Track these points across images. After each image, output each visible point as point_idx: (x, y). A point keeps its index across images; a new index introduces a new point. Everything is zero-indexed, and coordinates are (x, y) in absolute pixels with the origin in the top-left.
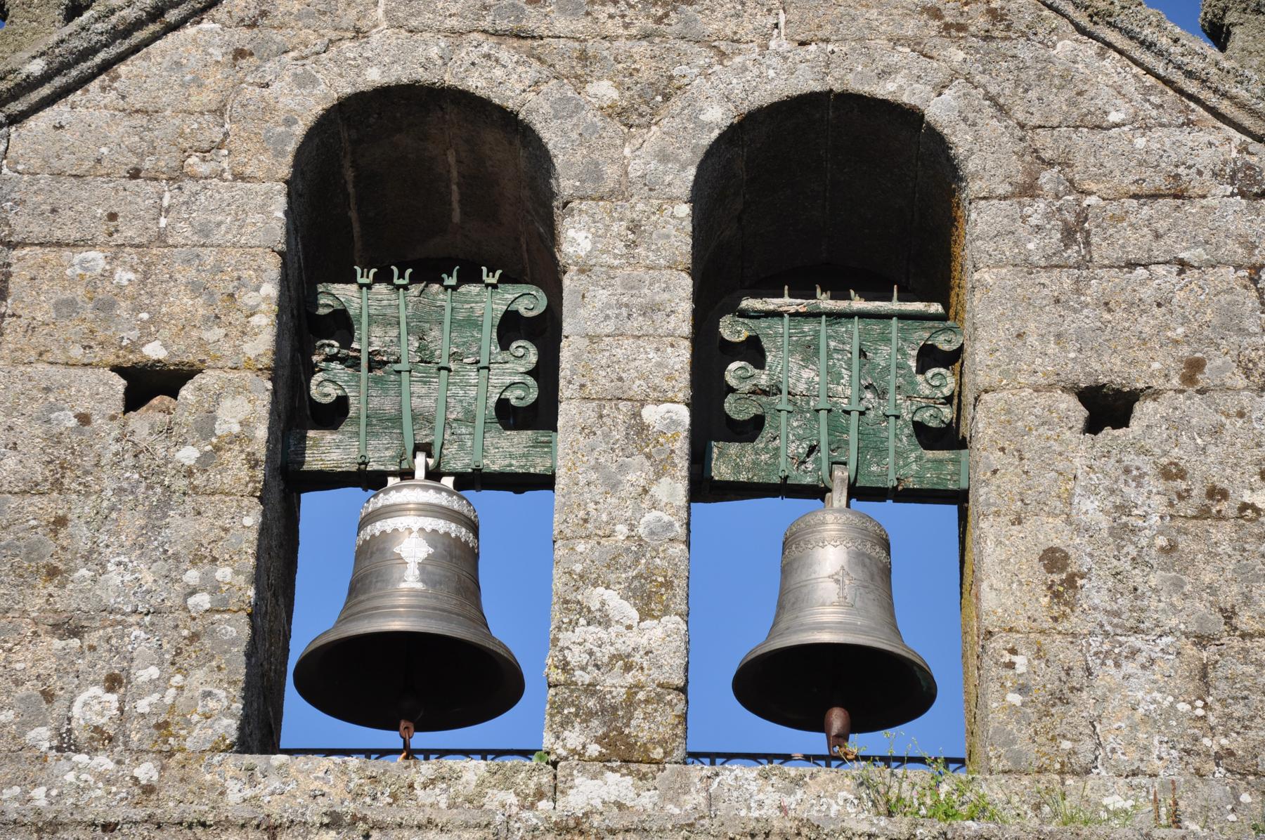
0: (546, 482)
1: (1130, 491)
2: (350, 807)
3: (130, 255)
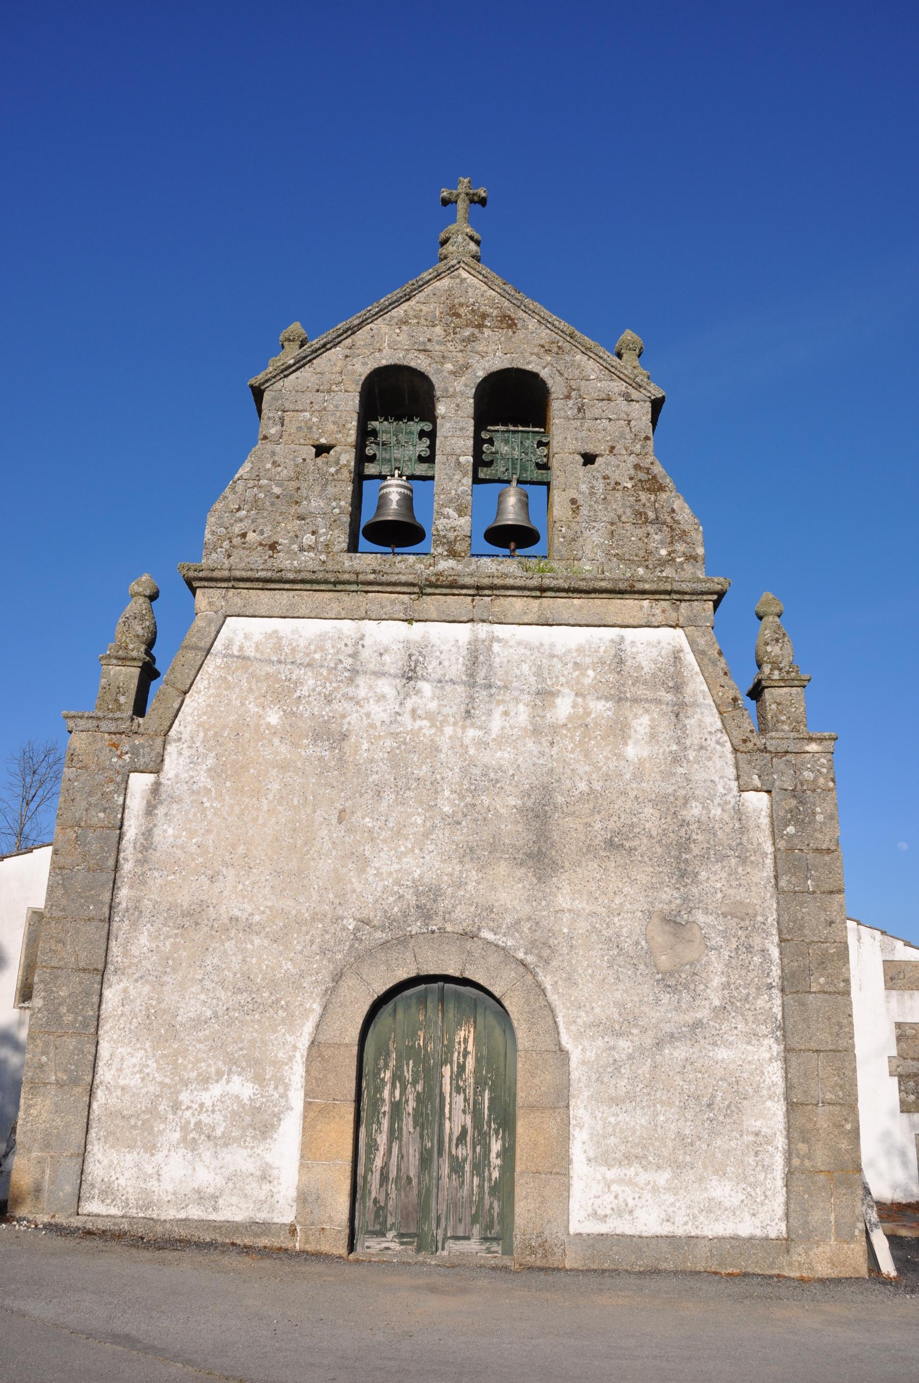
0: (432, 478)
1: (594, 482)
2: (378, 568)
3: (317, 414)
